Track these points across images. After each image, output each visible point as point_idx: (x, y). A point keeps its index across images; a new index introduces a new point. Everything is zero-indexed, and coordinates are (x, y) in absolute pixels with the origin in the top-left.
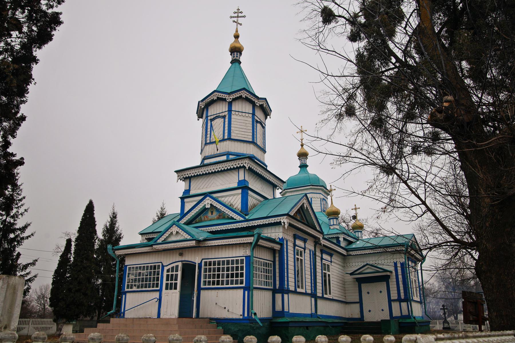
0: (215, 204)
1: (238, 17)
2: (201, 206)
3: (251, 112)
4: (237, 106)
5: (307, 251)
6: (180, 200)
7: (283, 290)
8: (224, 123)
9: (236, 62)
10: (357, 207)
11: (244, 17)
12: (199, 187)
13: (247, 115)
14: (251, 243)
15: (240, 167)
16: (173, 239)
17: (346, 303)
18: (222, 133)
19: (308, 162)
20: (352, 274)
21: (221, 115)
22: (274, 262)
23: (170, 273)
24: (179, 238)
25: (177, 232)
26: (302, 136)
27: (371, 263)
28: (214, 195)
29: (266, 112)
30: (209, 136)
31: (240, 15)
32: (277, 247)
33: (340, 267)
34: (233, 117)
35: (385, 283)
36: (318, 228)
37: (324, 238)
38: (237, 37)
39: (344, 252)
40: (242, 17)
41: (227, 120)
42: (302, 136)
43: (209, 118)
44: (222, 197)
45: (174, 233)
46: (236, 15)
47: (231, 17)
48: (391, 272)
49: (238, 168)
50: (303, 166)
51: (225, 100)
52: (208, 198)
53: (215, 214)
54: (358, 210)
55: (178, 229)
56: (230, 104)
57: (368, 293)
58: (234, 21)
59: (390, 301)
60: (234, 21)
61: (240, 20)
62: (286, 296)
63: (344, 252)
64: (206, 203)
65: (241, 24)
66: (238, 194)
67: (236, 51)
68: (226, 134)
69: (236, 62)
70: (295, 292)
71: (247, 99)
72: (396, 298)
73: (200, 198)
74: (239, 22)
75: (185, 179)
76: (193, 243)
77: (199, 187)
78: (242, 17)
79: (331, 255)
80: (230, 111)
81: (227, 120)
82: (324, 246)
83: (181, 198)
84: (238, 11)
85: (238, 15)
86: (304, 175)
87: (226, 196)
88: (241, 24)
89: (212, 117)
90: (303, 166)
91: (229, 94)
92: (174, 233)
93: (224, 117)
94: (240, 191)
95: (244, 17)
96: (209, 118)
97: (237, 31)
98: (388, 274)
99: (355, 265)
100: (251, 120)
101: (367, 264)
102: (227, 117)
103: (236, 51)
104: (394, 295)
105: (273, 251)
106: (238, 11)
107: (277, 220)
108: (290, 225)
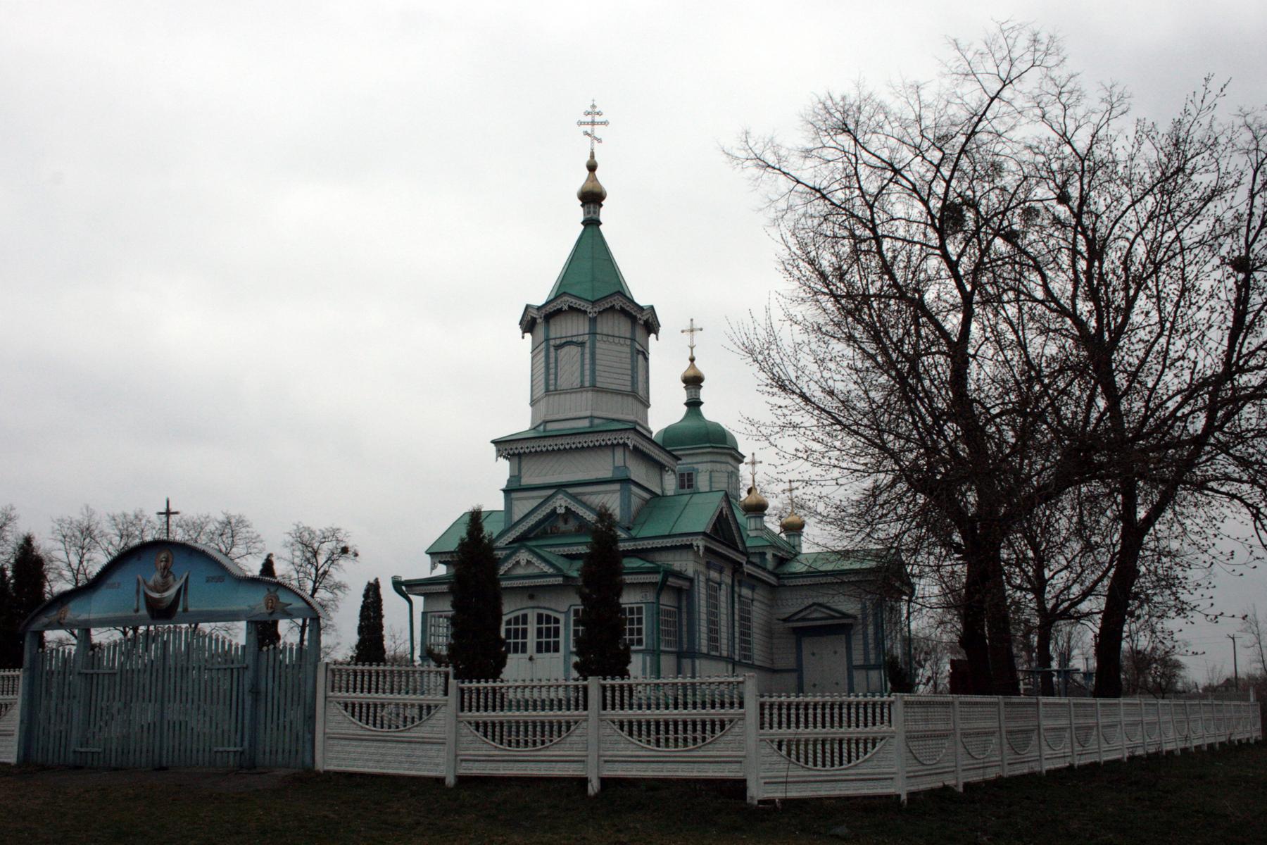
0: (576, 508)
1: (593, 123)
2: (546, 510)
3: (628, 335)
4: (605, 326)
5: (723, 586)
6: (502, 494)
7: (693, 654)
8: (583, 354)
9: (592, 223)
10: (697, 325)
11: (605, 123)
12: (537, 474)
13: (622, 341)
14: (656, 583)
15: (618, 444)
16: (520, 571)
17: (775, 671)
18: (577, 374)
19: (704, 394)
20: (785, 620)
21: (575, 339)
22: (679, 608)
23: (512, 627)
24: (530, 571)
25: (529, 562)
26: (692, 339)
27: (821, 600)
28: (571, 490)
29: (651, 326)
30: (552, 377)
31: (597, 118)
32: (685, 584)
33: (763, 607)
34: (598, 345)
35: (843, 637)
36: (741, 548)
37: (748, 562)
38: (592, 168)
39: (772, 580)
40: (601, 123)
41: (587, 350)
42: (692, 339)
43: (552, 343)
44: (584, 494)
45: (523, 562)
46: (589, 118)
47: (581, 123)
48: (855, 617)
49: (613, 446)
50: (694, 404)
51: (585, 312)
52: (560, 496)
53: (572, 525)
54: (697, 334)
55: (530, 557)
56: (593, 321)
57: (813, 654)
58: (586, 133)
59: (851, 668)
60: (586, 133)
61: (599, 131)
62: (697, 662)
63: (772, 580)
64: (557, 504)
65: (599, 141)
66: (614, 492)
67: (592, 198)
68: (587, 378)
69: (592, 223)
70: (707, 656)
71: (623, 311)
72: (861, 662)
73: (550, 492)
74: (597, 135)
75: (509, 457)
76: (560, 580)
77: (537, 474)
78: (601, 123)
79: (753, 589)
80: (593, 333)
81: (587, 350)
82: (749, 575)
83: (504, 491)
84: (593, 111)
85: (593, 119)
86: (693, 423)
87: (599, 493)
88: (599, 141)
89: (558, 342)
90: (694, 404)
91: (594, 303)
92: (523, 562)
93: (582, 344)
94: (617, 487)
95: (605, 123)
96: (552, 343)
97: (592, 156)
98: (850, 621)
99: (793, 604)
100: (628, 350)
101: (814, 604)
102: (588, 345)
103: (592, 198)
104: (858, 659)
105: (679, 591)
106: (593, 111)
107: (685, 541)
108: (707, 549)
